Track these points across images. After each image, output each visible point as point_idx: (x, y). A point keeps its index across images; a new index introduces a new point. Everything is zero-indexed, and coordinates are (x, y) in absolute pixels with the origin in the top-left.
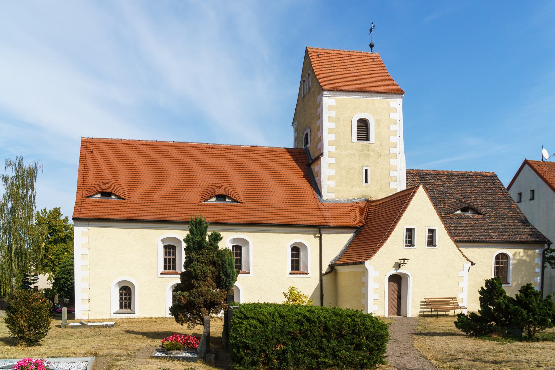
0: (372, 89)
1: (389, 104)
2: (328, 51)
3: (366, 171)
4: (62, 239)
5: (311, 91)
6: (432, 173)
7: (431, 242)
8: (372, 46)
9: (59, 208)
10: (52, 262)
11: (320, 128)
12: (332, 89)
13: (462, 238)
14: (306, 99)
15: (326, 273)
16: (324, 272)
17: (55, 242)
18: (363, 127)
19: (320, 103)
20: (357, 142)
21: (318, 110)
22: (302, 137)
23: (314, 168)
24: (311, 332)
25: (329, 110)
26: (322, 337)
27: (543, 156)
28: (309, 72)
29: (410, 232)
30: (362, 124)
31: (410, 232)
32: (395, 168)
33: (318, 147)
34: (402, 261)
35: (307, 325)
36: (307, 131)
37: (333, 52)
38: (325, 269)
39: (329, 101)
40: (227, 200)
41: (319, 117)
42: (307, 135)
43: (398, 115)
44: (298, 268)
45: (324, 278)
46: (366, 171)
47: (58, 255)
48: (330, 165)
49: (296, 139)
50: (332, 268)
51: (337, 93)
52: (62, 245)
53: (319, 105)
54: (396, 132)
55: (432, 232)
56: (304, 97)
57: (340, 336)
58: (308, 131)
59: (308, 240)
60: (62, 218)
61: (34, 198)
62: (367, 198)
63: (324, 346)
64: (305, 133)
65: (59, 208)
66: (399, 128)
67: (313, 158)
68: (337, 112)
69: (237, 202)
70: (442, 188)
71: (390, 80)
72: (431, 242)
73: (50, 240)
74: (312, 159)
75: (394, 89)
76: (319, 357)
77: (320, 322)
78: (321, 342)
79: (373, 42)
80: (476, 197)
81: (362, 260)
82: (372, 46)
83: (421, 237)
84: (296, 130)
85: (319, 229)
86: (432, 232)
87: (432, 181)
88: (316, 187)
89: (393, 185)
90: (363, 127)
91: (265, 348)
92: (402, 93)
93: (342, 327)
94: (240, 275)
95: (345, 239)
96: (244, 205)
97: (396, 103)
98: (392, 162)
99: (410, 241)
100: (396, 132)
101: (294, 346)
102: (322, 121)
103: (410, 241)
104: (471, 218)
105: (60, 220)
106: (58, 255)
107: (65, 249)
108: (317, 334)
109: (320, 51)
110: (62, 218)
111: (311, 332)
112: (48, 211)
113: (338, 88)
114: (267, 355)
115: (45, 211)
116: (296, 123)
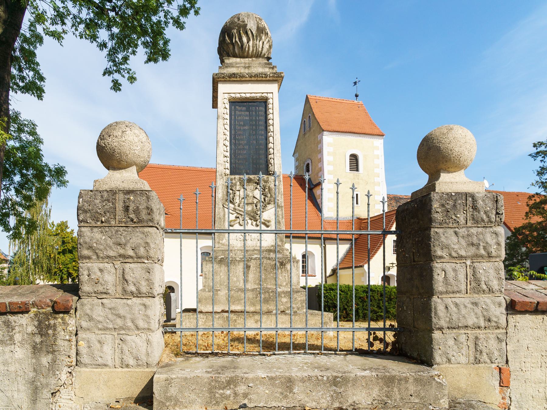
0: (360, 131)
2: (324, 99)
4: (69, 250)
5: (312, 130)
6: (405, 197)
8: (357, 96)
9: (66, 222)
10: (61, 271)
11: (321, 160)
12: (330, 130)
14: (306, 136)
15: (330, 276)
16: (328, 275)
17: (64, 252)
19: (320, 140)
21: (319, 146)
22: (303, 166)
23: (317, 191)
24: (373, 297)
26: (379, 300)
27: (279, 88)
28: (310, 115)
30: (353, 158)
33: (319, 175)
34: (391, 265)
35: (370, 293)
36: (308, 162)
37: (327, 99)
38: (329, 272)
39: (328, 139)
41: (320, 151)
42: (308, 165)
43: (380, 152)
45: (328, 279)
47: (67, 264)
49: (297, 168)
50: (334, 271)
51: (334, 133)
52: (69, 256)
53: (320, 142)
56: (305, 134)
57: (390, 299)
58: (310, 162)
59: (315, 249)
60: (69, 230)
61: (50, 212)
62: (358, 217)
63: (381, 306)
64: (306, 163)
65: (66, 222)
66: (381, 162)
67: (314, 184)
68: (334, 148)
71: (372, 123)
73: (59, 250)
74: (313, 184)
75: (376, 132)
76: (378, 312)
77: (378, 291)
78: (379, 303)
79: (358, 93)
81: (361, 264)
82: (357, 96)
84: (297, 160)
85: (325, 240)
88: (319, 208)
91: (346, 307)
92: (383, 135)
93: (391, 294)
95: (344, 248)
97: (379, 143)
101: (363, 306)
102: (323, 154)
105: (68, 233)
106: (67, 264)
107: (72, 259)
108: (376, 298)
109: (317, 98)
110: (69, 230)
111: (373, 297)
112: (55, 223)
113: (335, 129)
114: (346, 312)
115: (53, 224)
116: (297, 155)
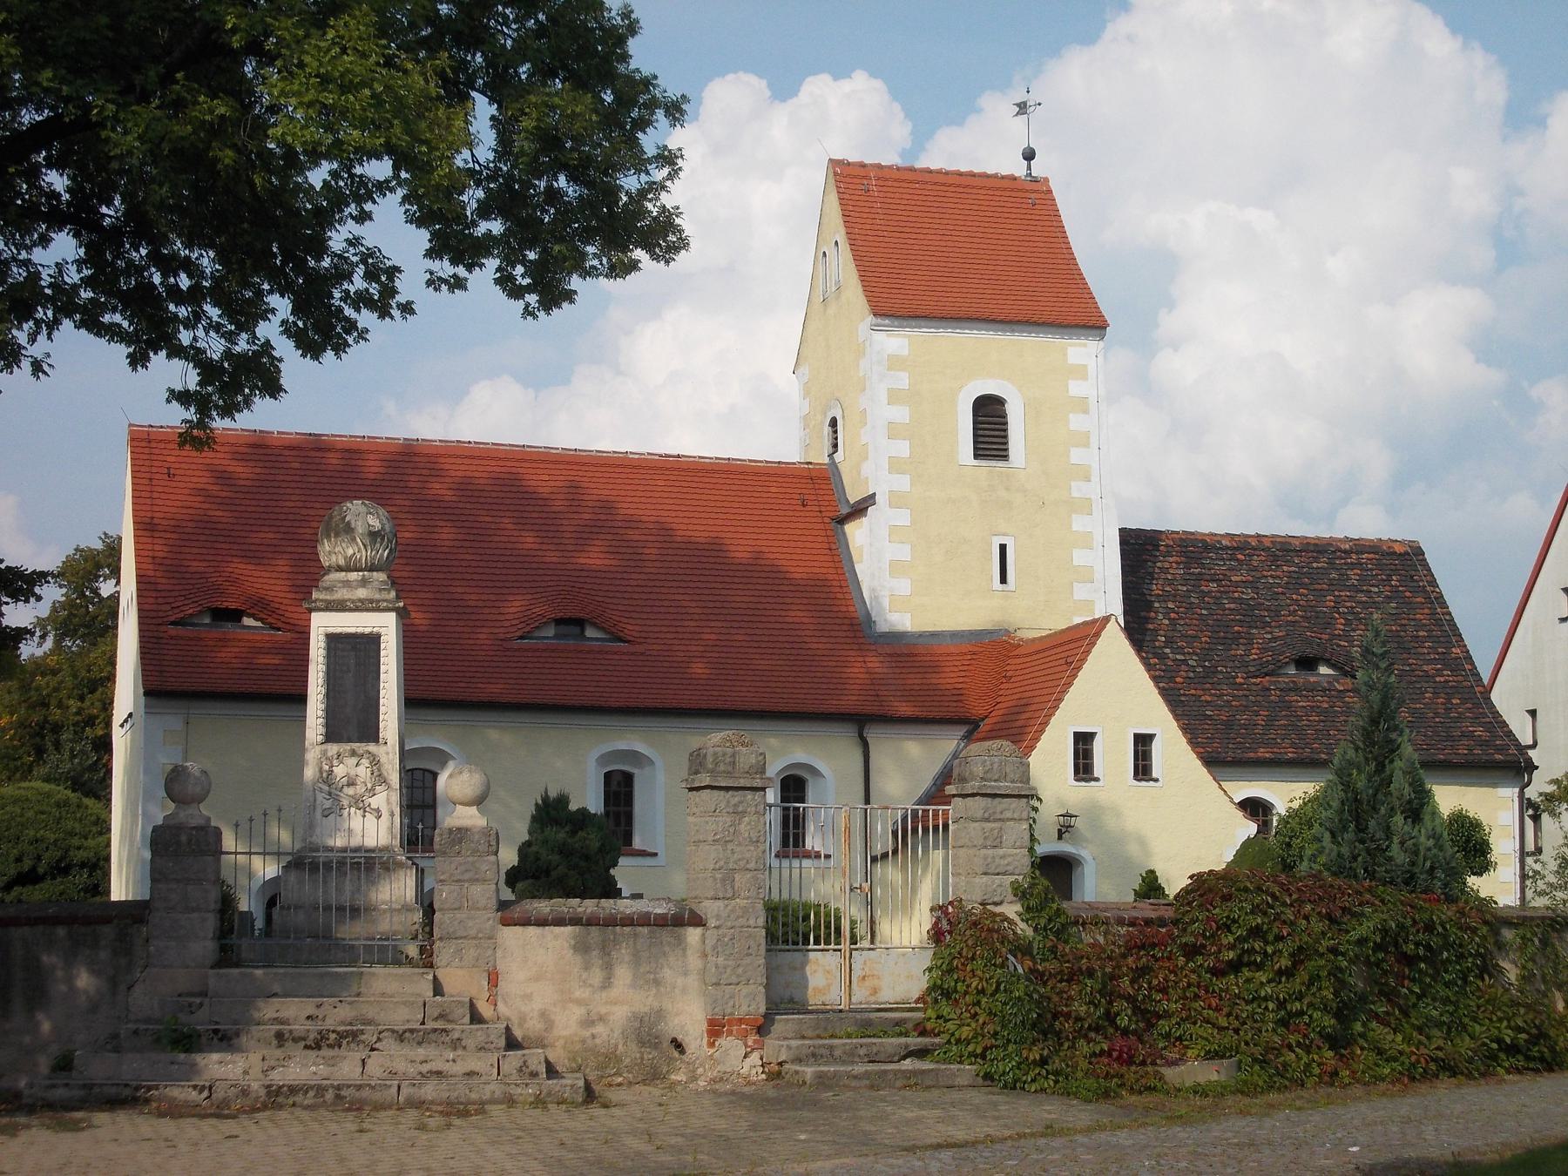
1: (1065, 355)
3: (1003, 548)
7: (1143, 770)
13: (1220, 758)
18: (990, 422)
20: (976, 463)
25: (889, 369)
29: (1083, 741)
31: (1083, 741)
32: (1086, 541)
40: (590, 632)
44: (799, 840)
46: (1003, 548)
48: (894, 529)
54: (1087, 435)
55: (1143, 743)
59: (828, 758)
69: (621, 640)
70: (1249, 594)
72: (1143, 770)
80: (1348, 623)
83: (1113, 757)
86: (1143, 743)
87: (1220, 568)
89: (1081, 592)
90: (990, 422)
94: (1494, 696)
96: (640, 648)
98: (1079, 523)
99: (1084, 767)
100: (1087, 435)
103: (1084, 767)
104: (1324, 690)
